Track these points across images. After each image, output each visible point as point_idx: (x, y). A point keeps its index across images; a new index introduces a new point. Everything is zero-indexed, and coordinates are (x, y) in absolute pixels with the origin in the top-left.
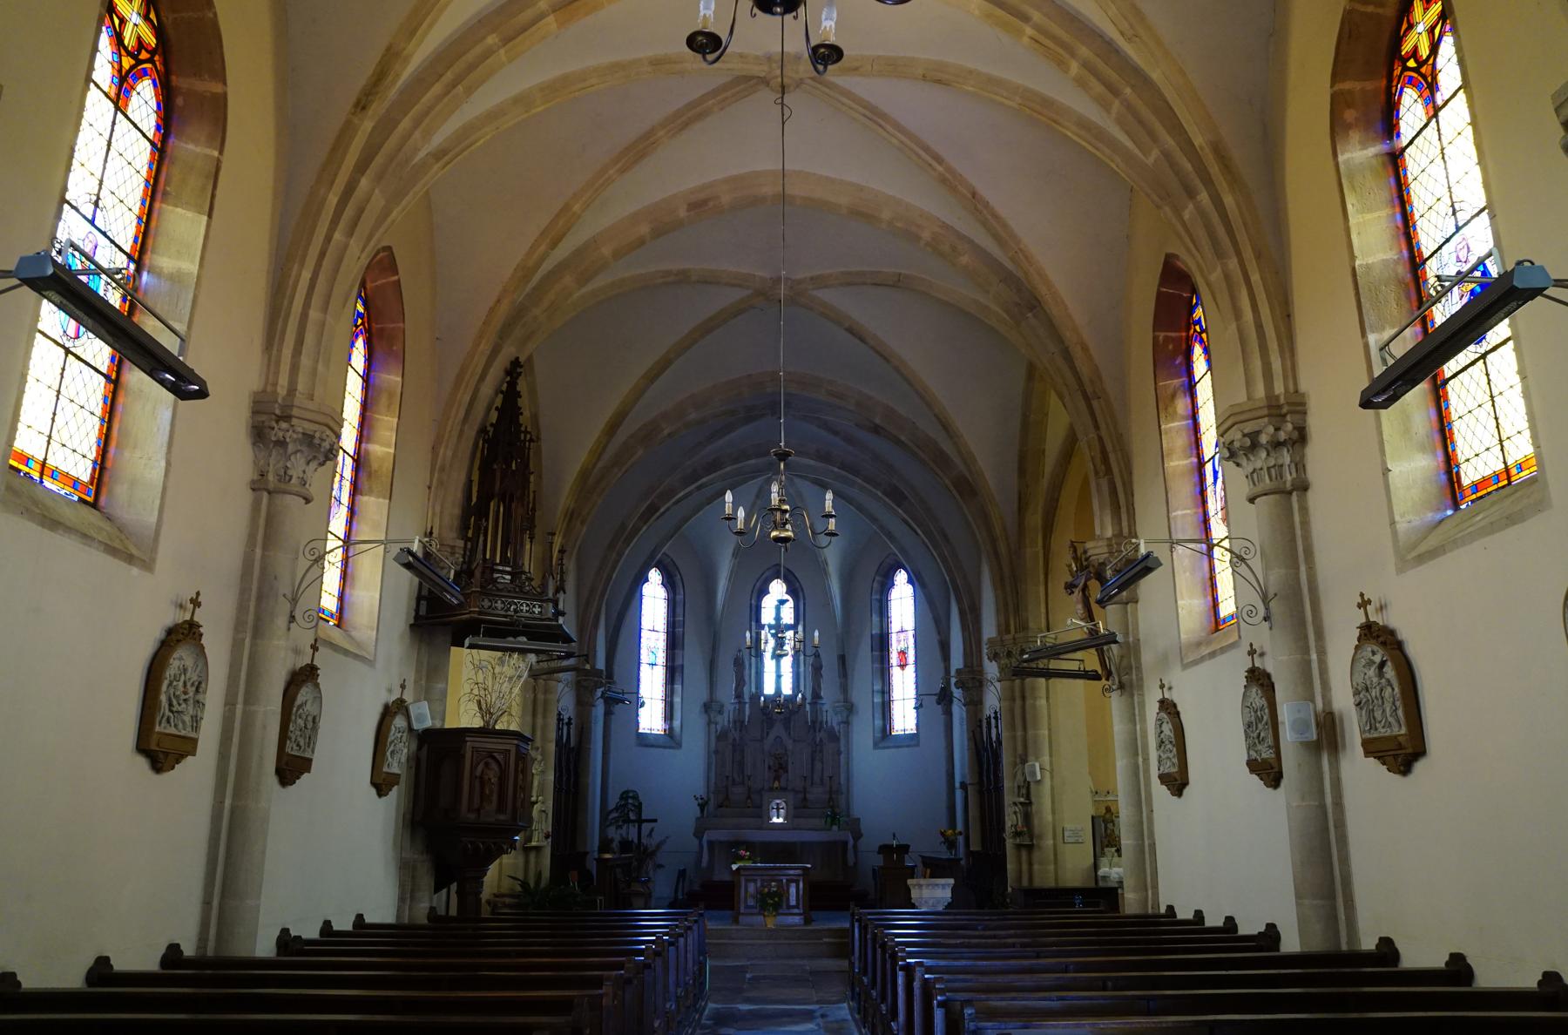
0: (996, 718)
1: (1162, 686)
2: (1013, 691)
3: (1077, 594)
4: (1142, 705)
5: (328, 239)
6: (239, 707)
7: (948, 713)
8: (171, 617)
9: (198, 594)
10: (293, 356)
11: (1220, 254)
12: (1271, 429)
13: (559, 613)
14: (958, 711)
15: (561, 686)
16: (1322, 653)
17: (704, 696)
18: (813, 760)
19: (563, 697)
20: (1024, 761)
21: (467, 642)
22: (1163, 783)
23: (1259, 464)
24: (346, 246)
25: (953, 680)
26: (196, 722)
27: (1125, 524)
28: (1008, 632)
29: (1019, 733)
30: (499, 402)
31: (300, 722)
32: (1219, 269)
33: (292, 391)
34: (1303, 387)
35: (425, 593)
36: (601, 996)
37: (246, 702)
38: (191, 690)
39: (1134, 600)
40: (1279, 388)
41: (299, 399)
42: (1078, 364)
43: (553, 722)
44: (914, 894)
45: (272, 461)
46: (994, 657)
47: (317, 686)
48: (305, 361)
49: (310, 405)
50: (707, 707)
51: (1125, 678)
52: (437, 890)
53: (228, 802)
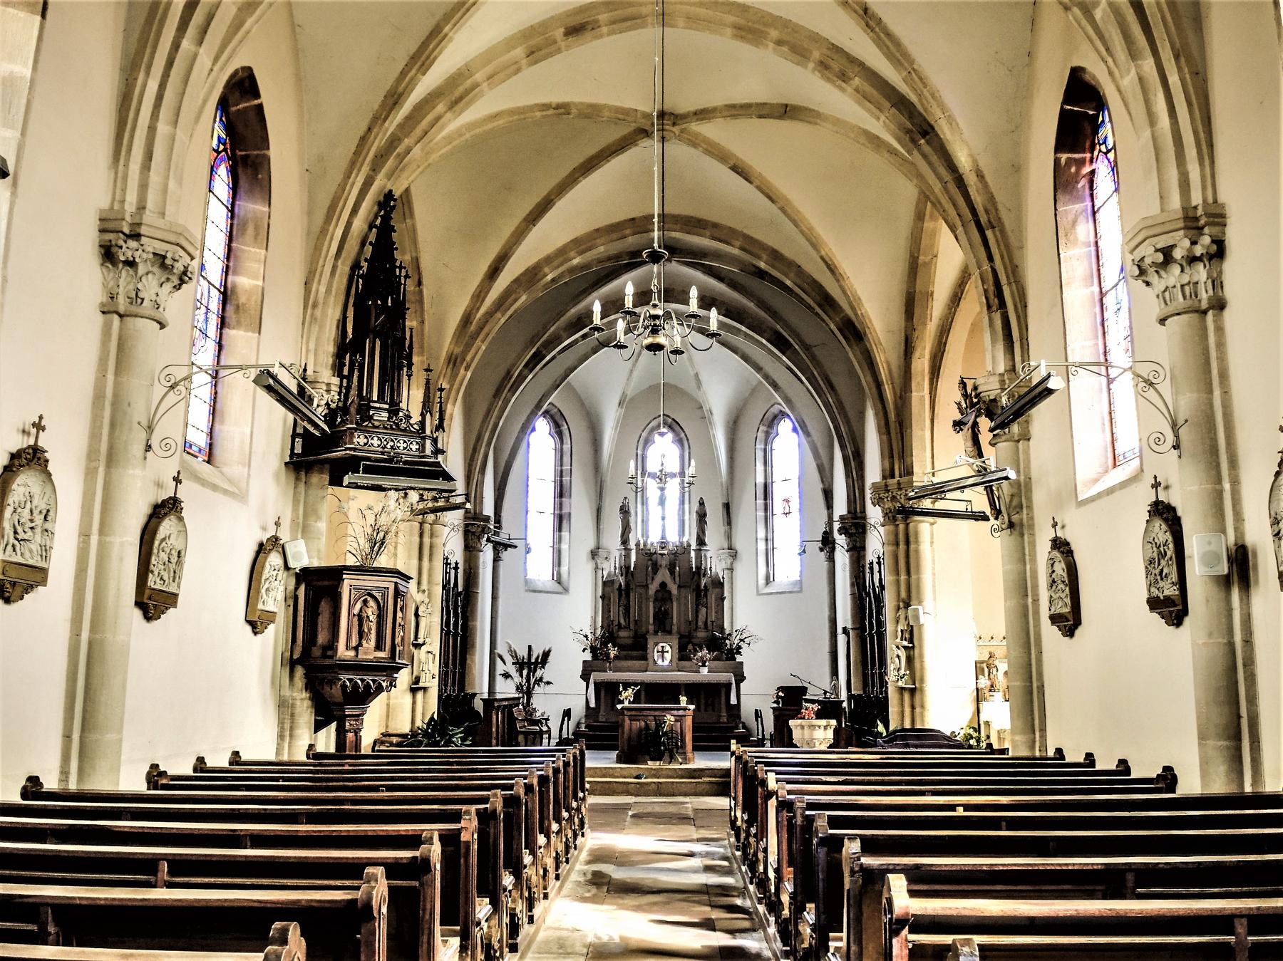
0: (879, 563)
1: (1055, 525)
2: (897, 535)
3: (967, 431)
4: (1033, 544)
5: (176, 46)
6: (94, 538)
7: (831, 559)
8: (18, 442)
9: (41, 418)
10: (141, 173)
11: (1133, 55)
12: (1187, 243)
13: (438, 451)
14: (842, 558)
15: (447, 530)
16: (1235, 482)
17: (591, 544)
18: (697, 606)
19: (451, 543)
20: (907, 605)
21: (346, 480)
22: (1053, 623)
23: (1171, 283)
24: (195, 57)
25: (836, 526)
26: (45, 552)
27: (1018, 358)
28: (893, 476)
29: (903, 577)
30: (372, 237)
31: (164, 556)
32: (1133, 72)
33: (141, 208)
34: (1222, 198)
35: (300, 430)
36: (459, 831)
37: (102, 532)
38: (39, 519)
39: (1026, 437)
40: (1196, 198)
41: (148, 217)
42: (973, 192)
43: (439, 565)
44: (796, 735)
45: (122, 282)
46: (878, 501)
47: (181, 519)
48: (155, 177)
49: (160, 223)
50: (594, 554)
51: (1015, 518)
52: (318, 726)
53: (85, 635)
